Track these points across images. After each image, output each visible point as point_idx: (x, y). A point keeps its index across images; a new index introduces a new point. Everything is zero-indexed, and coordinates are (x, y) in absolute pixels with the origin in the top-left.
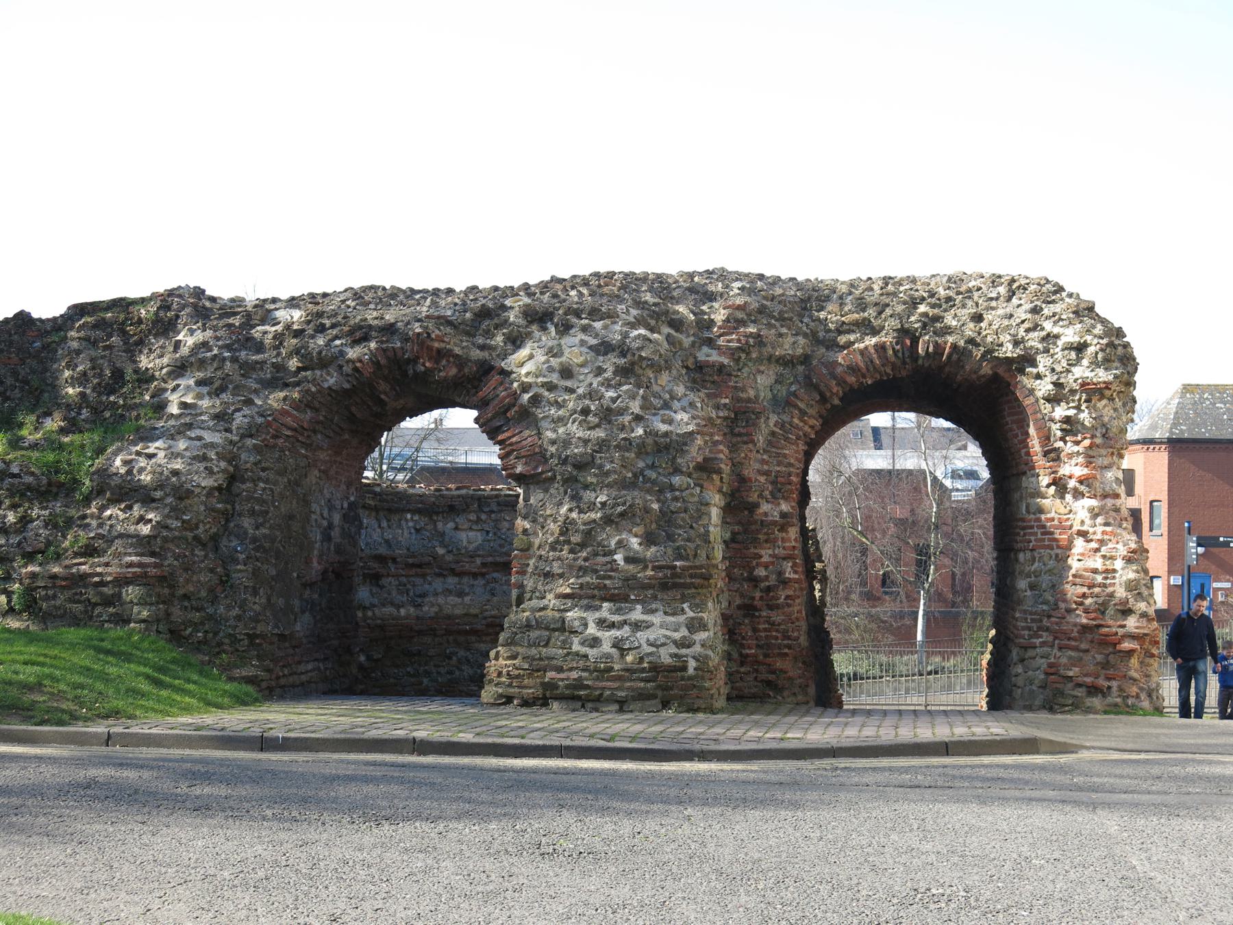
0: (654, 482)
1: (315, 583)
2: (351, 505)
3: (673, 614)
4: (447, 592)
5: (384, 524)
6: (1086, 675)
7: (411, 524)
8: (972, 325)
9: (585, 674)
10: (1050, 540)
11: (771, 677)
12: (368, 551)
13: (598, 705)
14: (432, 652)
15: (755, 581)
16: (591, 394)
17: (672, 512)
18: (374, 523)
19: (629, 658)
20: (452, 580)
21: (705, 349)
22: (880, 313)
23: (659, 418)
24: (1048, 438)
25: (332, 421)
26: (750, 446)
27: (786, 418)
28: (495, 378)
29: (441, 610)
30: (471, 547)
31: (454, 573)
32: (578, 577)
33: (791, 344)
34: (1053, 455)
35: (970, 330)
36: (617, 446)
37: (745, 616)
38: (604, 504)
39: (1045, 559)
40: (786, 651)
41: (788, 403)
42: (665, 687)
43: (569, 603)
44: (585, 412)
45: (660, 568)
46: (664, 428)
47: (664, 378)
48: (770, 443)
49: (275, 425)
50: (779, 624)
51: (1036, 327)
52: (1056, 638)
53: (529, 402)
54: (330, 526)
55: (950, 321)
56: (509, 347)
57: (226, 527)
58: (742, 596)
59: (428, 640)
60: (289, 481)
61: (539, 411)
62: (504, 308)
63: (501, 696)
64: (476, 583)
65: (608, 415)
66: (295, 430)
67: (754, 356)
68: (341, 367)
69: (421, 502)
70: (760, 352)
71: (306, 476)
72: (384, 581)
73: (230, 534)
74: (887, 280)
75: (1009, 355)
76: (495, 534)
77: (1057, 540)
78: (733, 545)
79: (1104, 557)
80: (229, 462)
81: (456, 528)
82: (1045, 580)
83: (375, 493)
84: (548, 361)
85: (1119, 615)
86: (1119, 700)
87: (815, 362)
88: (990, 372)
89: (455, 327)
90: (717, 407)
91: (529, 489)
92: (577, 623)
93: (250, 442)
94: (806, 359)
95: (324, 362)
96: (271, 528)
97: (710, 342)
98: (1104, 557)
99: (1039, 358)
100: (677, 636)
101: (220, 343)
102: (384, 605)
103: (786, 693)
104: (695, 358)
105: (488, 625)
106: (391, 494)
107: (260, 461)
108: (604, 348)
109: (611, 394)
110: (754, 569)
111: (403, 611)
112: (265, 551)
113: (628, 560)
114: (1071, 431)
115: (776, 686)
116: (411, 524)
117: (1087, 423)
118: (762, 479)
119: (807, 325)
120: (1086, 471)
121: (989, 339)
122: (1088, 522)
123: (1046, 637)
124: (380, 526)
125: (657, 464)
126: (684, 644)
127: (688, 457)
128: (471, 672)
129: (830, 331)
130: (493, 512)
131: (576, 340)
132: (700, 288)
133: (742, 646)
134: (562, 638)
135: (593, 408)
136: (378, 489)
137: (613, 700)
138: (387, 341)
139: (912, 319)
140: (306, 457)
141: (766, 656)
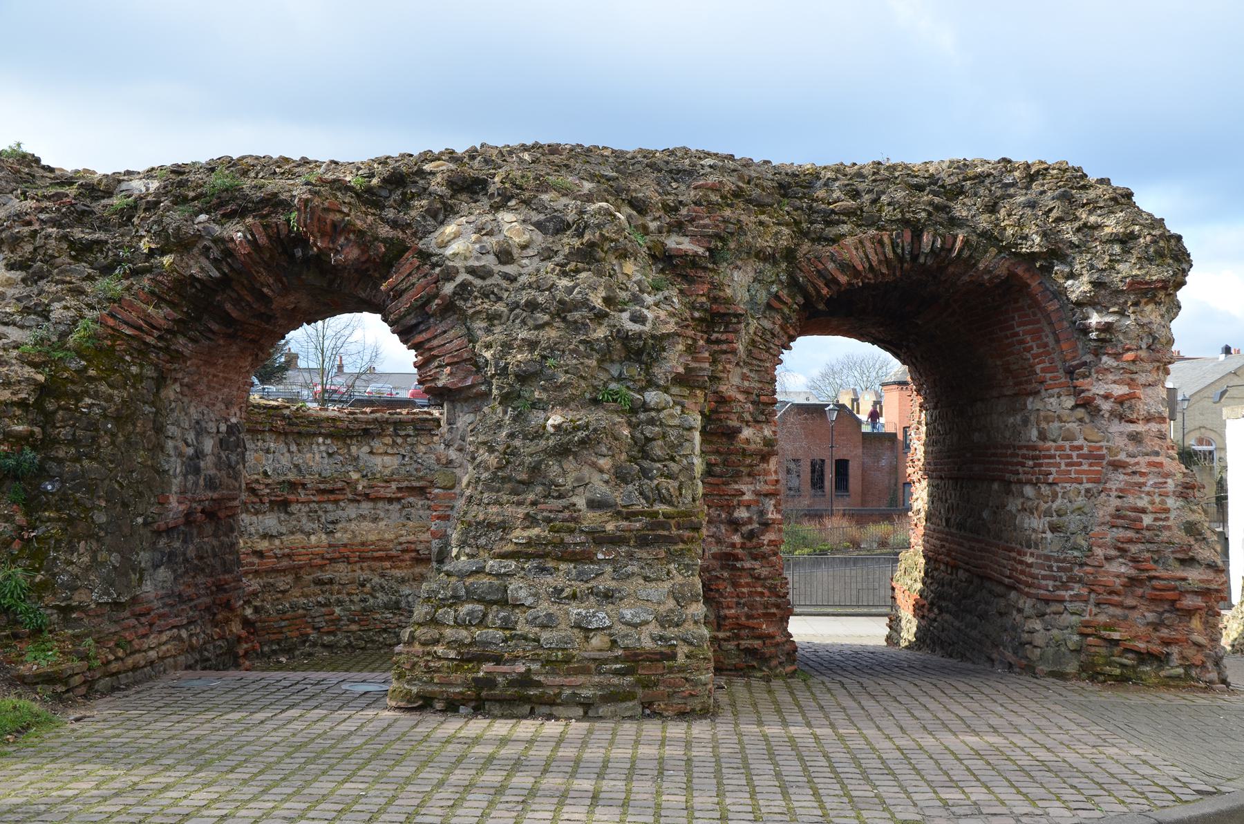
1: (176, 527)
2: (232, 429)
4: (362, 517)
5: (294, 448)
9: (535, 667)
10: (1077, 472)
11: (757, 643)
15: (735, 525)
20: (366, 507)
26: (729, 356)
30: (387, 472)
35: (984, 222)
37: (723, 568)
38: (558, 428)
40: (774, 610)
48: (749, 354)
52: (1092, 591)
54: (199, 454)
55: (960, 211)
56: (431, 222)
62: (421, 173)
64: (391, 507)
66: (139, 328)
67: (732, 245)
72: (294, 508)
76: (411, 458)
78: (710, 479)
81: (371, 453)
83: (284, 417)
84: (478, 241)
91: (454, 408)
94: (790, 255)
95: (182, 244)
102: (293, 533)
105: (403, 551)
111: (313, 538)
116: (323, 448)
123: (1077, 589)
124: (289, 451)
128: (386, 599)
130: (409, 436)
134: (502, 614)
136: (287, 412)
141: (749, 617)
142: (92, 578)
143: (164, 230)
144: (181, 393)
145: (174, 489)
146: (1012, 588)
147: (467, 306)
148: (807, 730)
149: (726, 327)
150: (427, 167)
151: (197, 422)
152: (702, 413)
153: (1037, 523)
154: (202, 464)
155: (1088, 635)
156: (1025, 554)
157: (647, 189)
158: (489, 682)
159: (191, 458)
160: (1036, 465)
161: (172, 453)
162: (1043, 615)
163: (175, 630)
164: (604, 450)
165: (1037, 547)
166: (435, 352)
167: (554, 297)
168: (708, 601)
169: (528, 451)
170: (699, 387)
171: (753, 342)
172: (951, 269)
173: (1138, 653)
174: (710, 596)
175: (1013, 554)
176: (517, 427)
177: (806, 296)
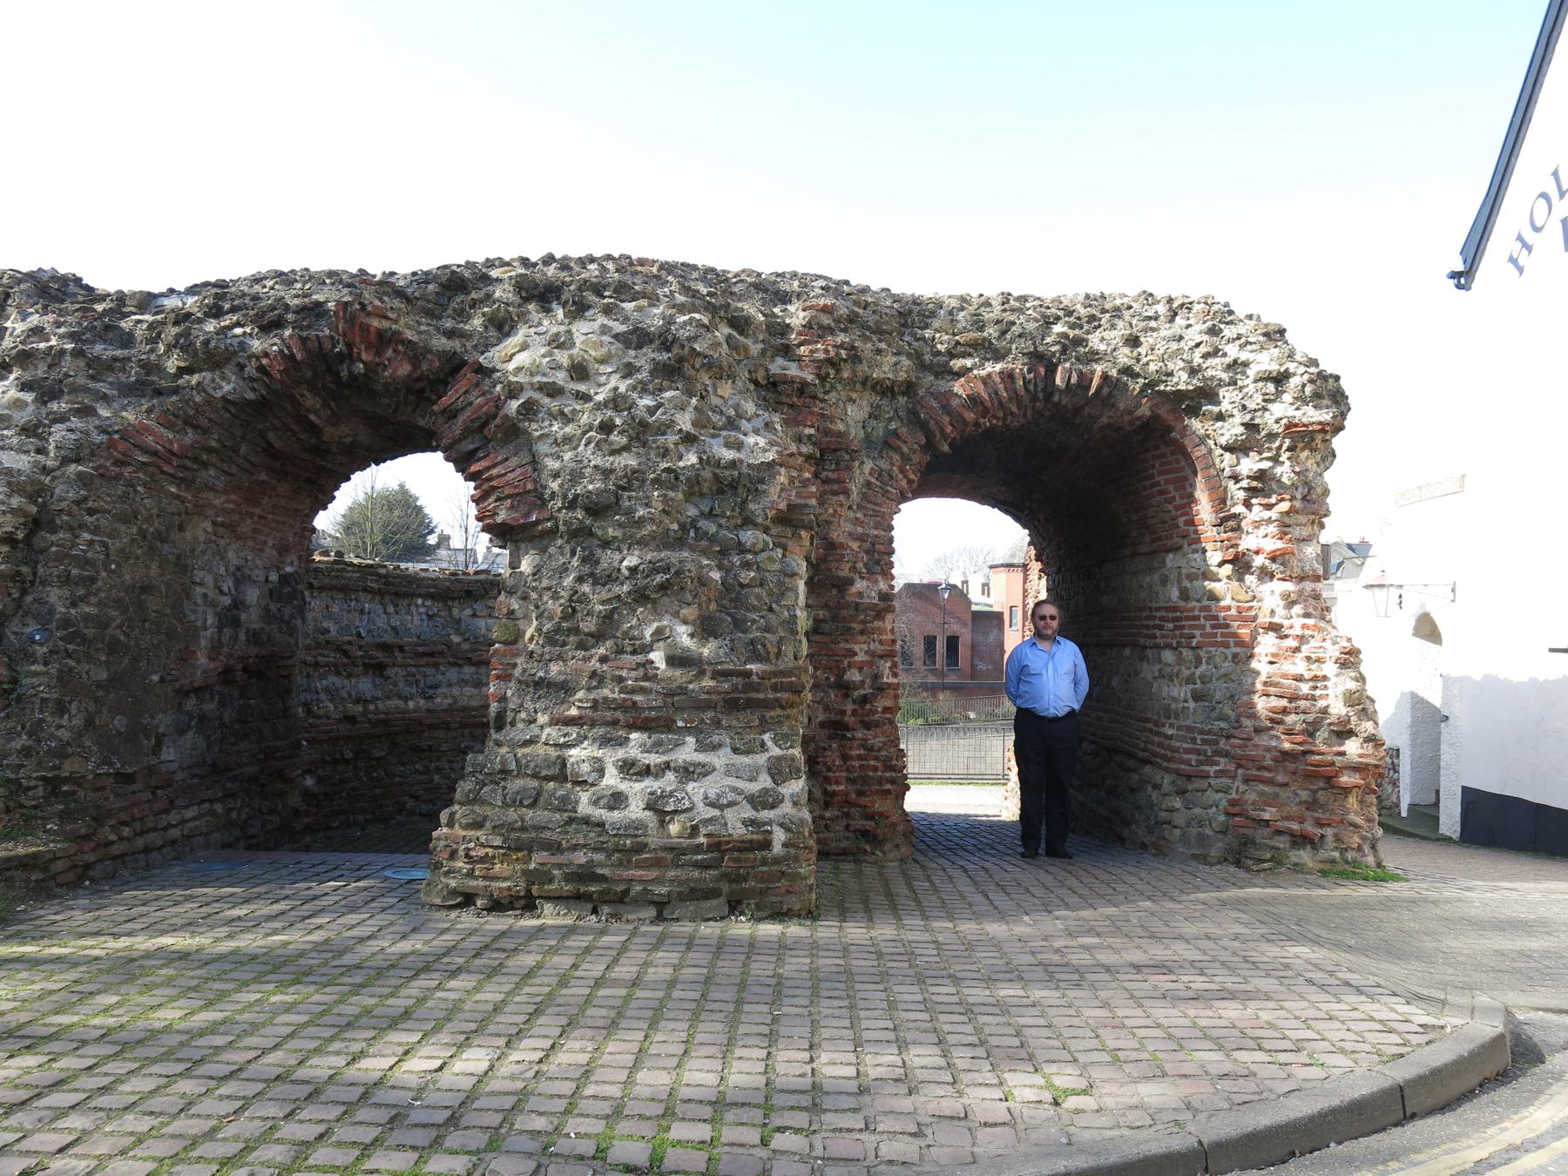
0: (713, 539)
2: (285, 579)
3: (748, 752)
5: (391, 609)
6: (1287, 818)
7: (422, 610)
8: (1126, 350)
9: (599, 857)
10: (1223, 635)
11: (869, 825)
12: (369, 639)
13: (621, 908)
14: (444, 747)
15: (845, 688)
16: (616, 402)
17: (742, 586)
18: (378, 608)
19: (674, 828)
21: (780, 361)
22: (1004, 333)
23: (721, 440)
24: (1223, 501)
25: (236, 451)
26: (841, 497)
27: (884, 465)
28: (466, 378)
29: (455, 702)
31: (470, 662)
32: (589, 689)
33: (890, 366)
34: (1229, 523)
35: (1124, 356)
36: (656, 481)
37: (831, 737)
38: (633, 570)
39: (1217, 660)
40: (889, 787)
41: (887, 444)
42: (732, 876)
43: (574, 732)
44: (606, 427)
45: (726, 674)
46: (729, 455)
47: (726, 389)
48: (864, 496)
49: (122, 446)
50: (879, 750)
51: (1215, 352)
52: (1239, 766)
53: (518, 412)
54: (238, 604)
55: (1095, 341)
56: (493, 333)
57: (18, 603)
58: (827, 708)
59: (441, 734)
60: (143, 534)
61: (534, 426)
62: (485, 279)
63: (454, 893)
65: (641, 433)
67: (846, 375)
68: (242, 367)
69: (435, 587)
70: (854, 371)
71: (181, 528)
72: (390, 672)
73: (26, 614)
74: (1006, 298)
75: (1182, 387)
77: (1235, 635)
78: (817, 637)
79: (1308, 658)
80: (32, 499)
81: (474, 615)
82: (1219, 689)
83: (379, 576)
84: (549, 354)
85: (1334, 738)
86: (1336, 854)
87: (921, 392)
88: (1148, 413)
89: (408, 300)
90: (799, 439)
91: (518, 549)
92: (585, 768)
93: (73, 468)
94: (909, 388)
96: (100, 604)
97: (786, 351)
98: (1308, 658)
99: (1222, 392)
100: (753, 787)
101: (62, 330)
102: (389, 698)
103: (888, 846)
104: (767, 370)
106: (399, 577)
107: (85, 499)
108: (637, 338)
109: (647, 401)
110: (845, 671)
111: (411, 704)
112: (85, 640)
113: (672, 661)
114: (1262, 490)
115: (875, 836)
116: (422, 610)
117: (1285, 480)
118: (855, 545)
119: (909, 344)
120: (1279, 545)
121: (1152, 367)
122: (1280, 611)
123: (1223, 763)
125: (717, 511)
126: (762, 801)
127: (766, 501)
129: (939, 353)
131: (596, 325)
132: (772, 290)
133: (827, 780)
135: (618, 421)
136: (383, 571)
137: (647, 900)
138: (309, 327)
139: (1048, 340)
140: (177, 497)
141: (860, 793)
142: (88, 744)
143: (192, 344)
144: (215, 534)
145: (203, 643)
146: (1148, 762)
147: (535, 429)
148: (926, 937)
149: (837, 464)
150: (494, 273)
151: (238, 569)
152: (807, 559)
153: (1180, 691)
154: (243, 616)
155: (1235, 815)
156: (1163, 725)
157: (751, 309)
158: (543, 876)
159: (228, 609)
160: (1176, 628)
161: (200, 601)
162: (1184, 792)
163: (207, 805)
164: (689, 598)
165: (1177, 717)
166: (494, 483)
167: (633, 419)
168: (812, 774)
169: (597, 600)
170: (804, 527)
171: (868, 484)
172: (1087, 410)
173: (1292, 834)
174: (815, 767)
175: (1150, 725)
176: (587, 569)
177: (929, 435)
